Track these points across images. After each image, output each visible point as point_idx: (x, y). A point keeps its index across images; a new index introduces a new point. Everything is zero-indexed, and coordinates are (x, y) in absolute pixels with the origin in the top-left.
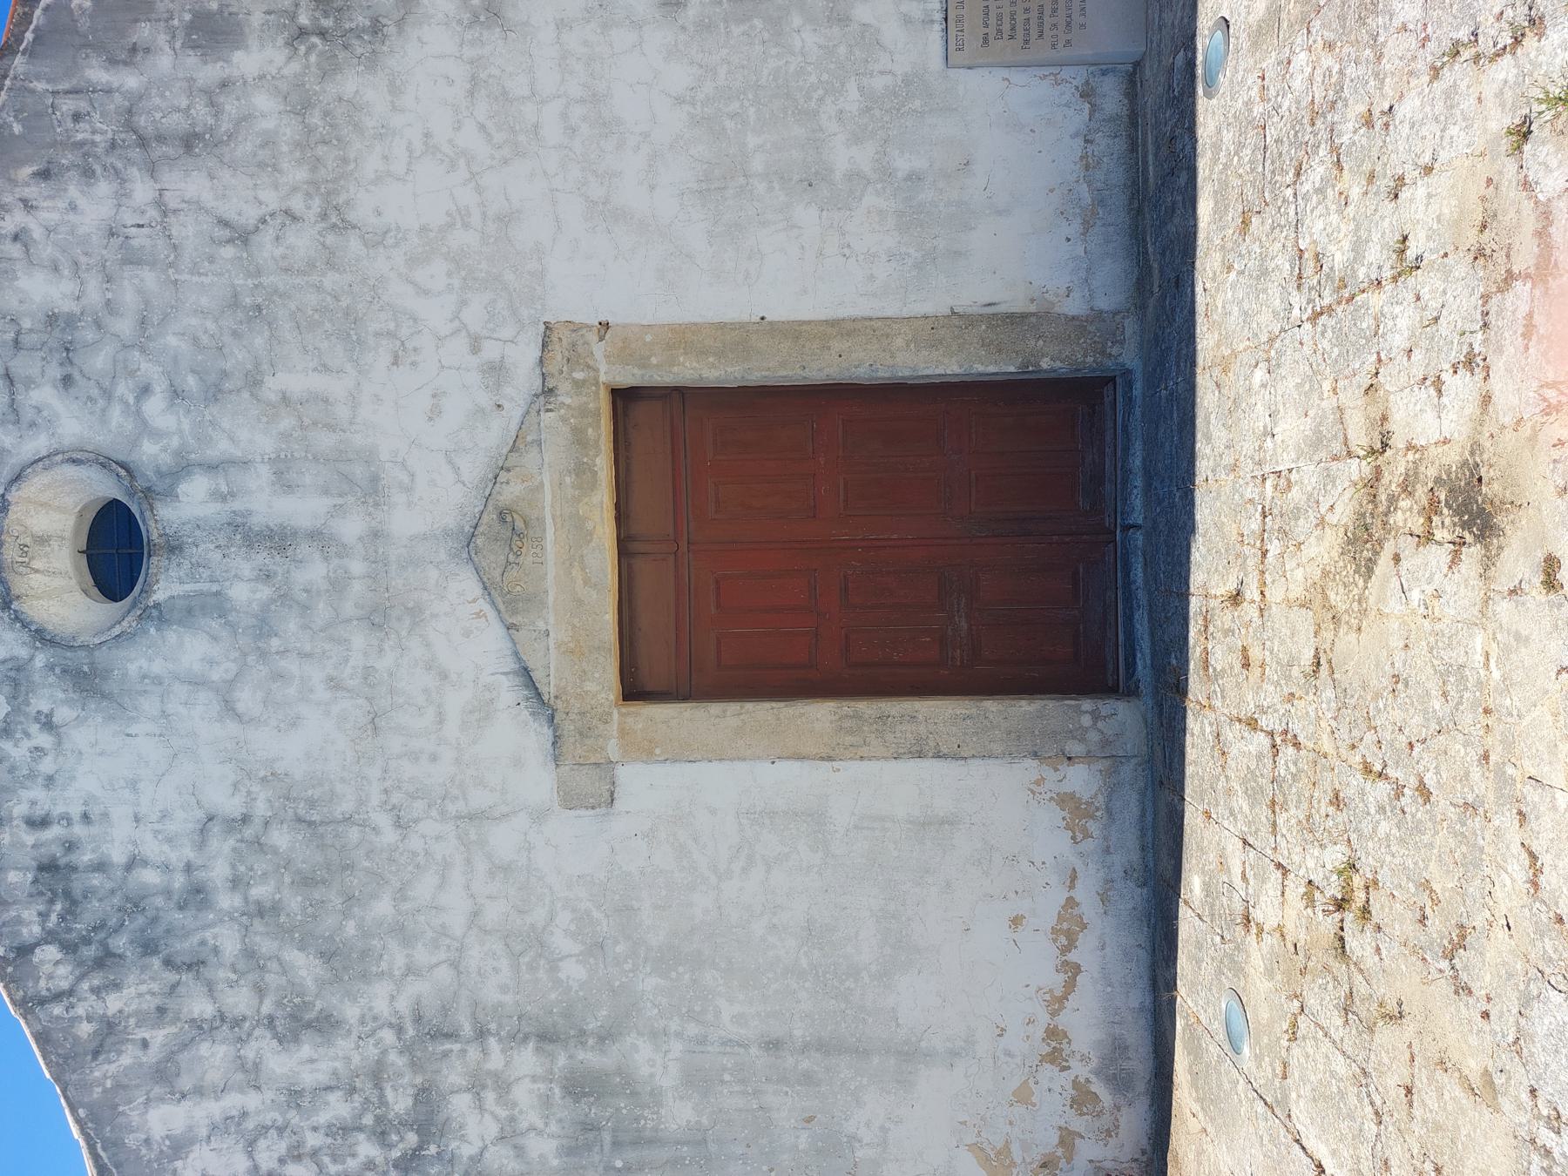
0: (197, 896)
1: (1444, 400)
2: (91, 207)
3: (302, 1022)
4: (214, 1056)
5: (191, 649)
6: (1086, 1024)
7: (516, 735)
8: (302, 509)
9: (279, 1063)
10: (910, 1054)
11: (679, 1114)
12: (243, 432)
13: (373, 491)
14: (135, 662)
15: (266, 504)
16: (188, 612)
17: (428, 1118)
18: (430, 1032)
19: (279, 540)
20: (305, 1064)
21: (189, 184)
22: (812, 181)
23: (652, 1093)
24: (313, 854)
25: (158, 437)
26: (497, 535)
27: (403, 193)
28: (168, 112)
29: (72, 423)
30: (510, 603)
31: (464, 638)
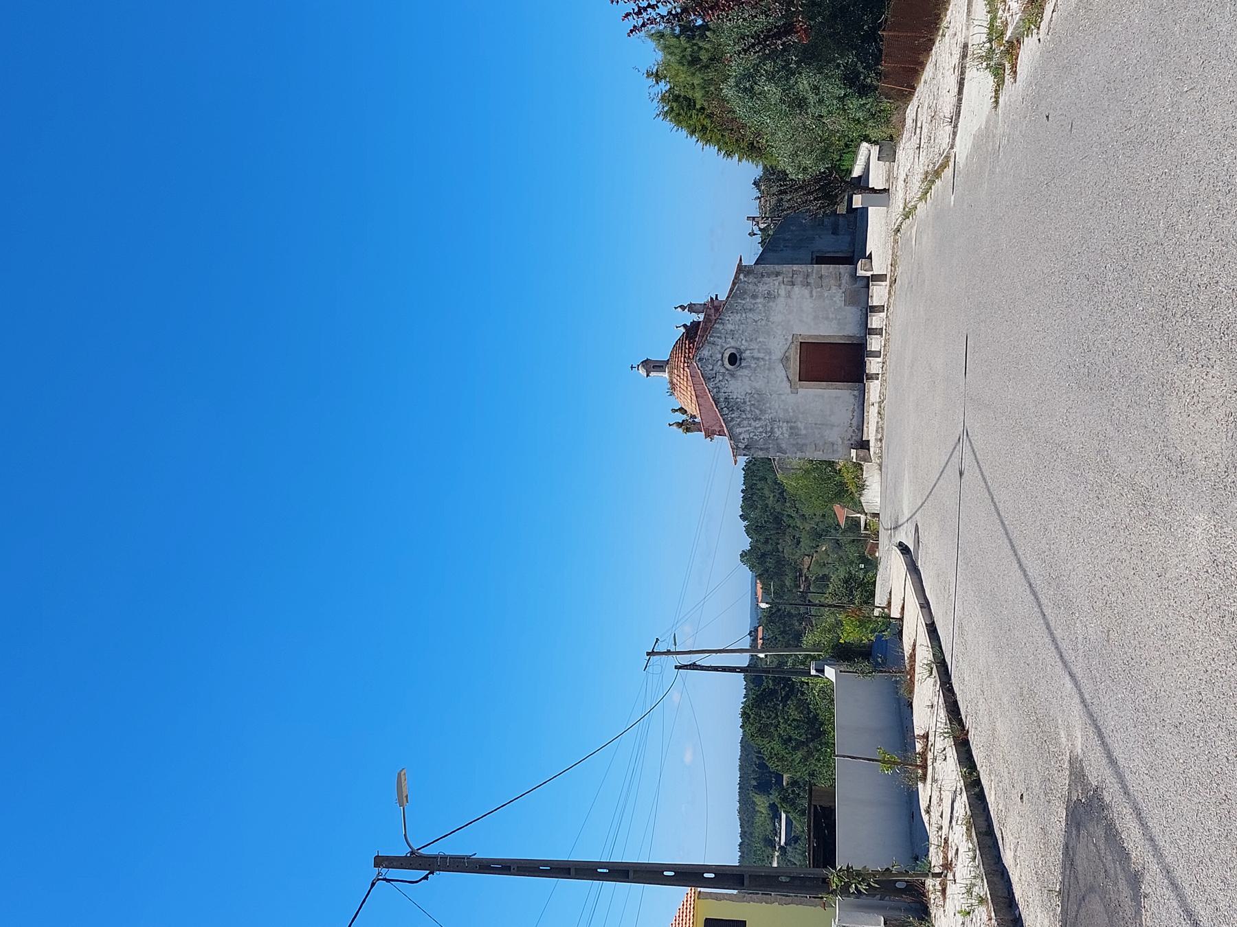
0: (745, 403)
1: (675, 427)
2: (738, 317)
3: (757, 419)
4: (745, 423)
5: (746, 372)
6: (855, 422)
7: (786, 384)
8: (761, 355)
9: (753, 424)
10: (833, 426)
11: (804, 432)
12: (754, 345)
13: (770, 353)
14: (739, 373)
15: (756, 355)
16: (746, 367)
17: (772, 431)
18: (773, 420)
19: (758, 359)
20: (757, 424)
21: (750, 315)
22: (827, 318)
23: (822, 690)
24: (759, 399)
25: (744, 345)
26: (785, 359)
27: (777, 318)
28: (748, 306)
29: (733, 344)
30: (786, 368)
31: (780, 373)
